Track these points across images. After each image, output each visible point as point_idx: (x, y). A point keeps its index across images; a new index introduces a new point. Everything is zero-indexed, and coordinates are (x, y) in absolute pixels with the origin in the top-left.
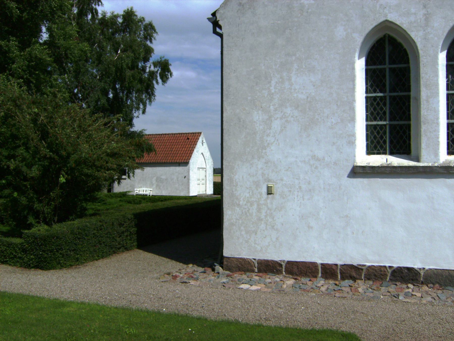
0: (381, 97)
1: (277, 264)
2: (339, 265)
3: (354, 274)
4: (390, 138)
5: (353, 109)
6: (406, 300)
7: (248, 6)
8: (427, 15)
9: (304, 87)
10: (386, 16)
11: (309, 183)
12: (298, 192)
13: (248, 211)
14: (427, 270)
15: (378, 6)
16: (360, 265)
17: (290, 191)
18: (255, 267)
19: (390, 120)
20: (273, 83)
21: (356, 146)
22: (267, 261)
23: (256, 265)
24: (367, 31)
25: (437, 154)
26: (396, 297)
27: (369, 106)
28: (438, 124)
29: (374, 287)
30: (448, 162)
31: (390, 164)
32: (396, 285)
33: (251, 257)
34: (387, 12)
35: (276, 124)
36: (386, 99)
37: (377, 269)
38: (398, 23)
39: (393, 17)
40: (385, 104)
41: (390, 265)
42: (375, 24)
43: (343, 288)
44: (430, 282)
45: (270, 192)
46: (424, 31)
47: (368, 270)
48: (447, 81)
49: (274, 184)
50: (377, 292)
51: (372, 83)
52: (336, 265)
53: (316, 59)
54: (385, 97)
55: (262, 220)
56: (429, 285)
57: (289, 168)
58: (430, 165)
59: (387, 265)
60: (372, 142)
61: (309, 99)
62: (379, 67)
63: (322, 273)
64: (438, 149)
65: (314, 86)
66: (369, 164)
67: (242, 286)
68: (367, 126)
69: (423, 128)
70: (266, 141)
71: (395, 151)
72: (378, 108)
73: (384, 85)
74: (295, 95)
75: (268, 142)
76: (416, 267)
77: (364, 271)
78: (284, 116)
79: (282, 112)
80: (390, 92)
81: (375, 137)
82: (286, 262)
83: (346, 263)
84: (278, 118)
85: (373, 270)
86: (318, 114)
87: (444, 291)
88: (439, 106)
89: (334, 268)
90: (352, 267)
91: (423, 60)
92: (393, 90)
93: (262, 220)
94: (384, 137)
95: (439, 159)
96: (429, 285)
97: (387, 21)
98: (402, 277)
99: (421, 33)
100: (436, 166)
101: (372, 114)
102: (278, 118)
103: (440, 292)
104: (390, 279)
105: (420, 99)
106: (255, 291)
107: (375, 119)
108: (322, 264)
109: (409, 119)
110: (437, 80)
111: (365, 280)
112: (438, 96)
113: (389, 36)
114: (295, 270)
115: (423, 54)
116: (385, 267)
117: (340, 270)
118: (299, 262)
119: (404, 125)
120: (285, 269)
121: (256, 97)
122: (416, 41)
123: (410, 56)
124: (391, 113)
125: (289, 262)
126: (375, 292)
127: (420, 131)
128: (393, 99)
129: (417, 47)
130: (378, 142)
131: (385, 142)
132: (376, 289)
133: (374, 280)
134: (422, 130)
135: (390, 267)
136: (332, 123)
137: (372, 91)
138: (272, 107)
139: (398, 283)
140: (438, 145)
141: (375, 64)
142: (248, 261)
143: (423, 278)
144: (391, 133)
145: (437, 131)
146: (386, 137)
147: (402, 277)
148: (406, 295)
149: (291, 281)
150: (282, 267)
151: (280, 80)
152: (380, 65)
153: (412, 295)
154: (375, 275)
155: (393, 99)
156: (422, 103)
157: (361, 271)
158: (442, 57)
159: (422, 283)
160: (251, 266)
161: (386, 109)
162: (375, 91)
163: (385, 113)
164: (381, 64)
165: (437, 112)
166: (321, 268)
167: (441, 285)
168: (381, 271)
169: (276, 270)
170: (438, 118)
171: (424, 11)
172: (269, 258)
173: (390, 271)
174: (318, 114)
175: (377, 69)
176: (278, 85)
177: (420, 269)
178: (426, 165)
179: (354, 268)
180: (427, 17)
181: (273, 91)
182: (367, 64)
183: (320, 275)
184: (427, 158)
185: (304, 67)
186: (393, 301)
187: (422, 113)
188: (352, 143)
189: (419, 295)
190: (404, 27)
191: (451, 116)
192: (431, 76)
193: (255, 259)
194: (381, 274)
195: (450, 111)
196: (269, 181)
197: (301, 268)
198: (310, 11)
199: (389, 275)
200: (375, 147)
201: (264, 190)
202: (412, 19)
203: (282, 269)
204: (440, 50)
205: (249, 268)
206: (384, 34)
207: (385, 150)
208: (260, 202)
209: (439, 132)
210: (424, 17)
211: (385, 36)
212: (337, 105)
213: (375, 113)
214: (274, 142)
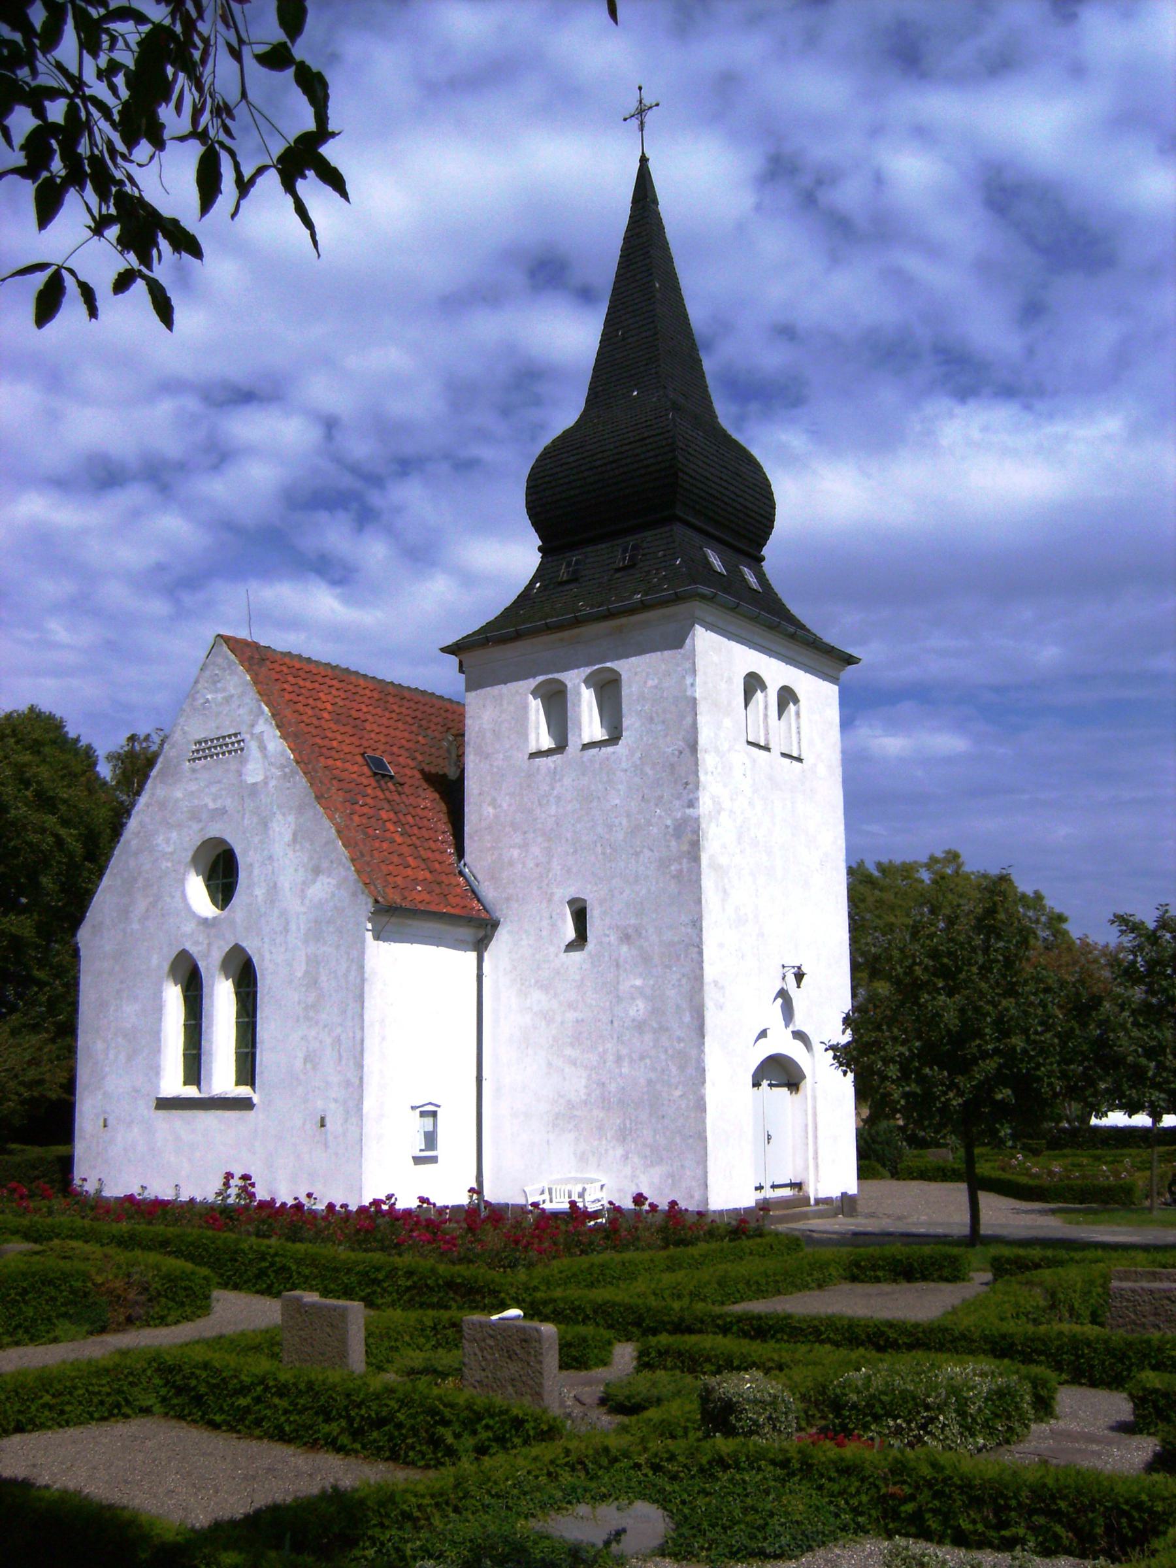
24: (172, 959)
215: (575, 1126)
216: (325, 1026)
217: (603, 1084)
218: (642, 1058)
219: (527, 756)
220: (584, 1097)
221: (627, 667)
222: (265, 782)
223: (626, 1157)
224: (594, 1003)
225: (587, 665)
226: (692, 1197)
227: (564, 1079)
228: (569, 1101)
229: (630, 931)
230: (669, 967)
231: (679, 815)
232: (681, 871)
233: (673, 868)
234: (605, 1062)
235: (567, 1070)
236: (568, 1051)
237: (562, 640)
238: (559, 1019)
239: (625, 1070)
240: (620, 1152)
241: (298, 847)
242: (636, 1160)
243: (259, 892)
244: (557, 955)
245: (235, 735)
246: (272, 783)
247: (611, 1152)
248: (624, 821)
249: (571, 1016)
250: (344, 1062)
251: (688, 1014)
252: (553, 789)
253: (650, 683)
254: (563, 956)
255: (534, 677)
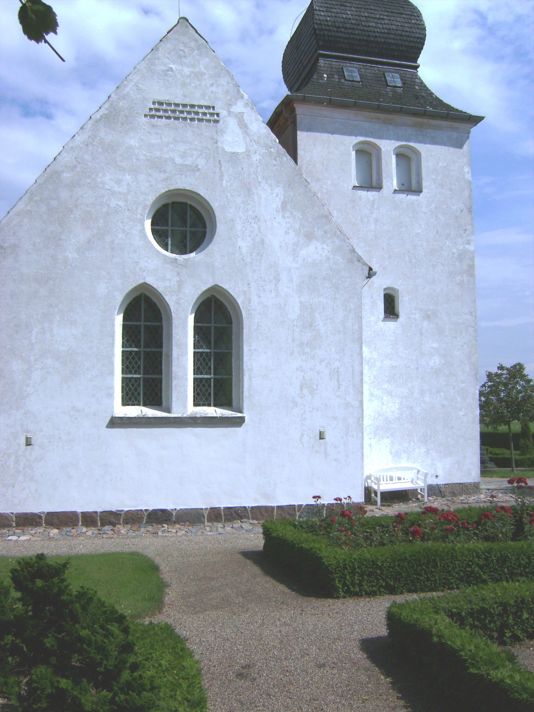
0: (136, 351)
1: (37, 517)
2: (99, 512)
3: (113, 520)
4: (144, 390)
5: (112, 363)
6: (164, 535)
7: (9, 251)
8: (180, 283)
9: (65, 339)
10: (145, 278)
11: (69, 434)
12: (58, 442)
13: (5, 463)
14: (178, 510)
15: (138, 269)
16: (119, 511)
17: (50, 442)
18: (13, 522)
19: (144, 374)
20: (34, 333)
21: (114, 398)
22: (26, 514)
23: (14, 519)
24: (127, 291)
25: (185, 406)
26: (156, 534)
27: (125, 359)
28: (186, 379)
29: (134, 528)
30: (195, 413)
31: (145, 415)
32: (153, 526)
33: (8, 512)
34: (146, 275)
35: (36, 375)
36: (140, 354)
37: (134, 513)
38: (155, 286)
39: (151, 281)
40: (139, 359)
41: (146, 508)
42: (134, 285)
43: (107, 532)
44: (180, 521)
45: (28, 442)
46: (177, 296)
47: (126, 514)
48: (194, 341)
49: (33, 435)
50: (138, 532)
51: (128, 338)
52: (96, 512)
53: (78, 313)
54: (140, 352)
55: (20, 472)
56: (181, 524)
57: (49, 418)
58: (180, 416)
59: (144, 508)
60: (127, 394)
61: (70, 352)
62: (135, 323)
63: (82, 522)
64: (187, 402)
65: (75, 339)
66: (126, 415)
67: (10, 538)
68: (123, 378)
69: (174, 383)
70: (26, 391)
71: (148, 403)
72: (133, 362)
73: (139, 341)
74: (56, 347)
75: (27, 392)
76: (169, 508)
77: (123, 516)
78: (44, 367)
79: (42, 363)
80: (145, 347)
81: (130, 390)
82: (45, 514)
83: (106, 510)
84: (38, 368)
85: (131, 514)
86: (79, 367)
87: (194, 526)
88: (187, 364)
89: (94, 515)
90: (111, 513)
91: (176, 322)
92: (147, 346)
93: (20, 472)
94: (139, 389)
95: (187, 411)
96: (181, 524)
97: (145, 283)
98: (156, 519)
99: (174, 298)
100: (185, 417)
101: (127, 367)
102: (38, 368)
103: (190, 528)
104: (146, 521)
105: (172, 356)
106: (25, 540)
107: (130, 373)
108: (82, 513)
109: (161, 373)
110: (187, 341)
111: (123, 525)
112: (187, 355)
113: (145, 295)
114: (56, 520)
115: (175, 317)
116: (141, 510)
117: (100, 516)
118: (59, 512)
119: (156, 378)
120: (45, 520)
121: (16, 346)
122: (170, 304)
123: (164, 318)
124: (145, 367)
125: (48, 513)
126: (136, 532)
127: (172, 386)
128: (147, 354)
129: (170, 310)
130: (133, 394)
131: (139, 394)
132: (136, 530)
133: (132, 523)
134: (173, 384)
135: (146, 510)
136: (92, 375)
137: (128, 346)
138: (32, 358)
139: (154, 525)
140: (187, 398)
141: (131, 320)
142: (5, 516)
143: (176, 518)
144: (144, 386)
145: (186, 386)
146: (140, 390)
147: (156, 519)
148: (163, 532)
149: (55, 531)
150: (42, 519)
151: (42, 331)
152: (136, 321)
153: (168, 531)
154: (133, 519)
155: (147, 354)
156: (173, 361)
157: (119, 516)
158: (191, 319)
159: (175, 522)
160: (9, 521)
161: (140, 363)
162: (131, 346)
163: (139, 367)
164: (137, 321)
165: (185, 368)
166: (82, 516)
167: (190, 523)
168: (138, 515)
169: (36, 522)
170: (186, 375)
171: (177, 278)
172: (29, 511)
173: (146, 514)
174: (79, 367)
175: (134, 325)
176: (39, 335)
177: (172, 510)
178: (177, 416)
179: (113, 514)
180: (180, 284)
181: (34, 341)
182: (124, 319)
183: (80, 523)
184: (177, 410)
185: (66, 319)
186: (155, 537)
187: (173, 369)
188: (110, 395)
189: (175, 531)
190: (161, 290)
191: (197, 372)
192: (182, 337)
193: (12, 513)
194: (139, 518)
195: (196, 367)
196: (28, 432)
197: (61, 518)
198: (74, 264)
199: (145, 518)
200: (130, 399)
201: (23, 441)
202: (167, 284)
203: (42, 521)
204: (189, 314)
205: (6, 523)
206: (140, 293)
207: (139, 401)
208: (18, 453)
209: (187, 387)
210: (178, 284)
211: (141, 295)
212: (97, 358)
213: (130, 367)
214: (34, 392)
215: (391, 434)
216: (322, 361)
217: (412, 407)
218: (438, 392)
219: (393, 191)
220: (397, 416)
221: (424, 149)
222: (248, 154)
223: (427, 452)
224: (404, 355)
225: (398, 139)
226: (470, 474)
227: (383, 404)
228: (386, 418)
229: (429, 313)
230: (456, 338)
231: (461, 248)
232: (463, 281)
233: (458, 278)
234: (412, 394)
235: (385, 398)
236: (385, 386)
237: (378, 118)
238: (378, 364)
239: (427, 399)
240: (423, 450)
241: (287, 214)
242: (434, 454)
243: (244, 245)
244: (376, 323)
245: (208, 107)
246: (256, 158)
247: (417, 450)
248: (425, 244)
249: (387, 362)
250: (343, 388)
251: (467, 366)
252: (372, 213)
253: (441, 164)
254: (381, 324)
255: (356, 135)
